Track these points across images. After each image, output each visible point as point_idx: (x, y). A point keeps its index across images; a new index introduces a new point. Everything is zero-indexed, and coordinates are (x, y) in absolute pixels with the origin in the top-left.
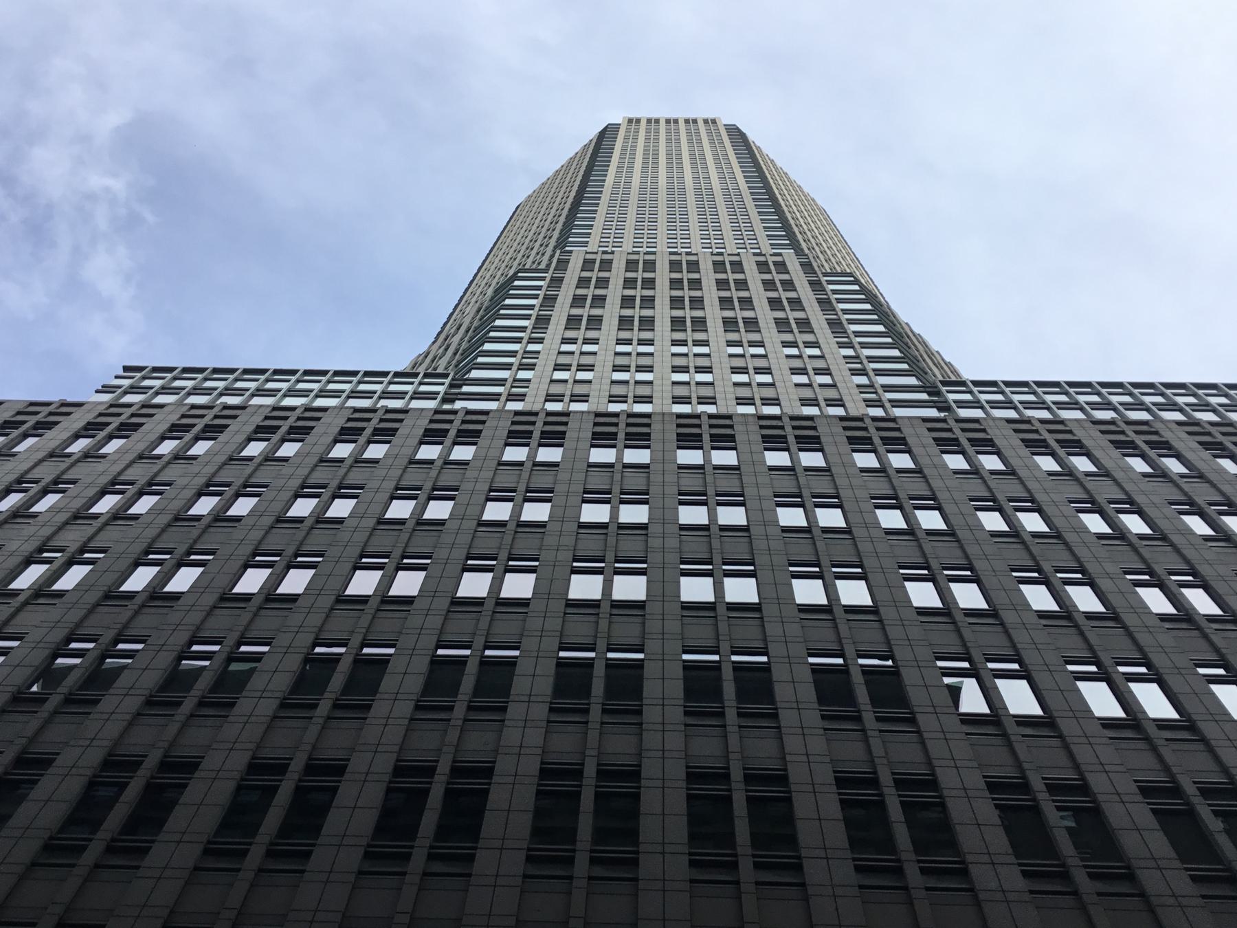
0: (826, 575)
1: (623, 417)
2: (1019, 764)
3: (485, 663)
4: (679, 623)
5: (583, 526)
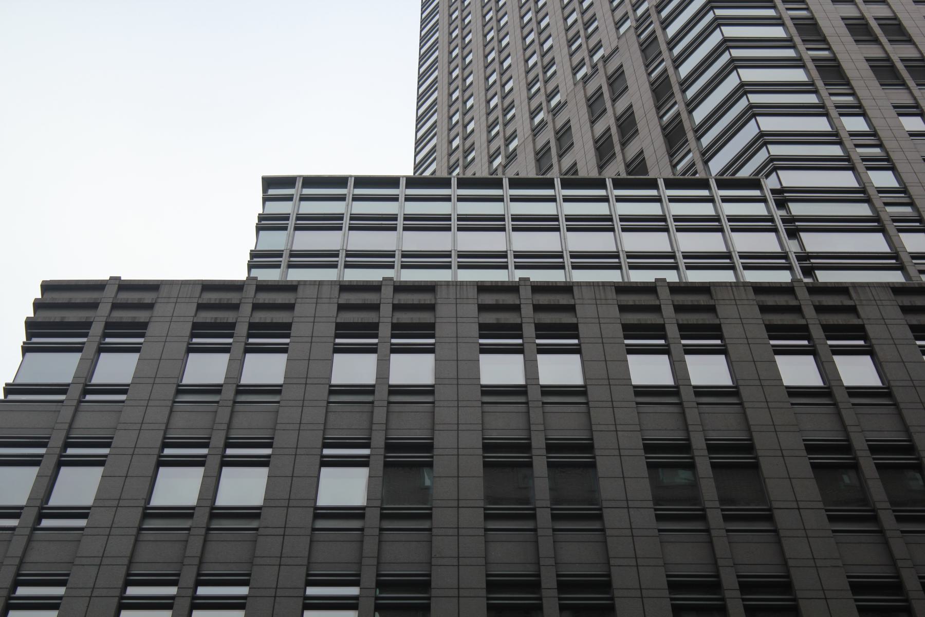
1: (387, 292)
2: (893, 561)
5: (337, 390)
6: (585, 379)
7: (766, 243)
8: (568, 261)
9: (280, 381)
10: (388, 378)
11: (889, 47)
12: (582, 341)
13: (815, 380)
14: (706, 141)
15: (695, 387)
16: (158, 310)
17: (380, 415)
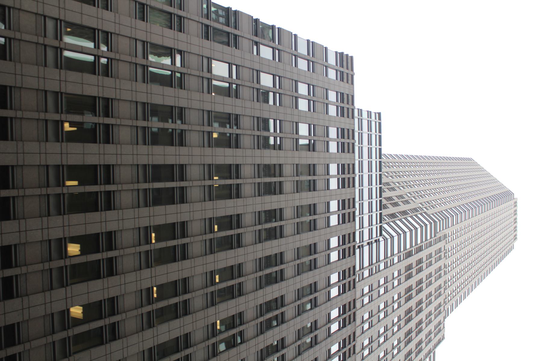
0: (339, 248)
7: (366, 237)
8: (361, 202)
11: (415, 290)
13: (332, 282)
14: (392, 223)
16: (347, 84)
17: (322, 139)
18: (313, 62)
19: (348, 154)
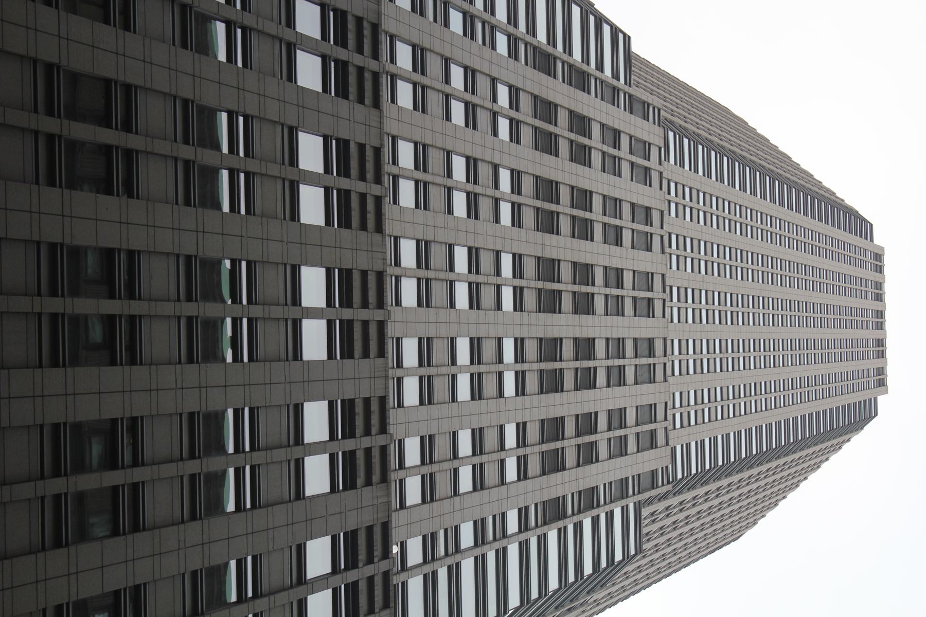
0: (338, 577)
3: (211, 174)
4: (282, 403)
6: (311, 498)
9: (303, 220)
10: (307, 318)
12: (343, 494)
15: (305, 544)
16: (359, 107)
18: (244, 30)
19: (363, 234)
